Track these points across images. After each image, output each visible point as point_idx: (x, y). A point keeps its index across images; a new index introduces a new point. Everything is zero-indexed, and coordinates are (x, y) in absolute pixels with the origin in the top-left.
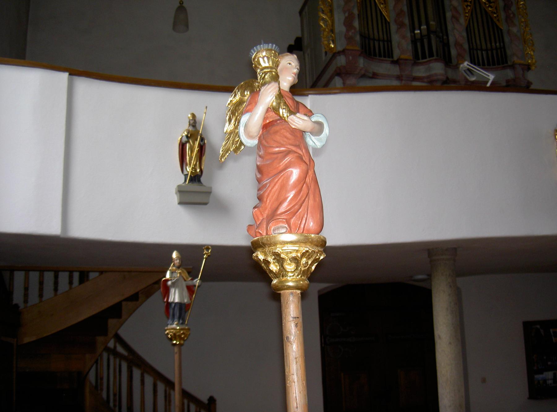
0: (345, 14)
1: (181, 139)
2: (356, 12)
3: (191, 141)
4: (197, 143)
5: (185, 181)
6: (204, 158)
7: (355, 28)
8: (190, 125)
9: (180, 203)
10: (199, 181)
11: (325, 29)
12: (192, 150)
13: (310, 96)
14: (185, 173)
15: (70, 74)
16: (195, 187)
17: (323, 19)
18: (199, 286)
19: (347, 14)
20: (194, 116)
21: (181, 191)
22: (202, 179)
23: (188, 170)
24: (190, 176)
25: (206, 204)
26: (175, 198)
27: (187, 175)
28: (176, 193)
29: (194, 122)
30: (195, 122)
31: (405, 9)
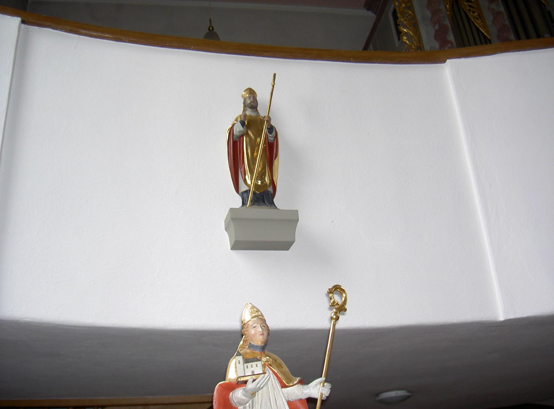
0: (434, 27)
1: (231, 130)
2: (447, 23)
3: (250, 132)
4: (261, 142)
5: (244, 204)
6: (275, 162)
7: (451, 43)
8: (245, 106)
9: (237, 246)
10: (272, 203)
11: (411, 46)
12: (254, 146)
13: (448, 61)
14: (243, 188)
15: (23, 22)
16: (262, 212)
17: (406, 34)
18: (323, 402)
19: (437, 27)
20: (251, 92)
21: (234, 219)
22: (275, 200)
23: (249, 182)
24: (254, 193)
25: (286, 246)
26: (225, 240)
27: (247, 192)
28: (227, 229)
29: (251, 101)
30: (255, 101)
31: (507, 22)
